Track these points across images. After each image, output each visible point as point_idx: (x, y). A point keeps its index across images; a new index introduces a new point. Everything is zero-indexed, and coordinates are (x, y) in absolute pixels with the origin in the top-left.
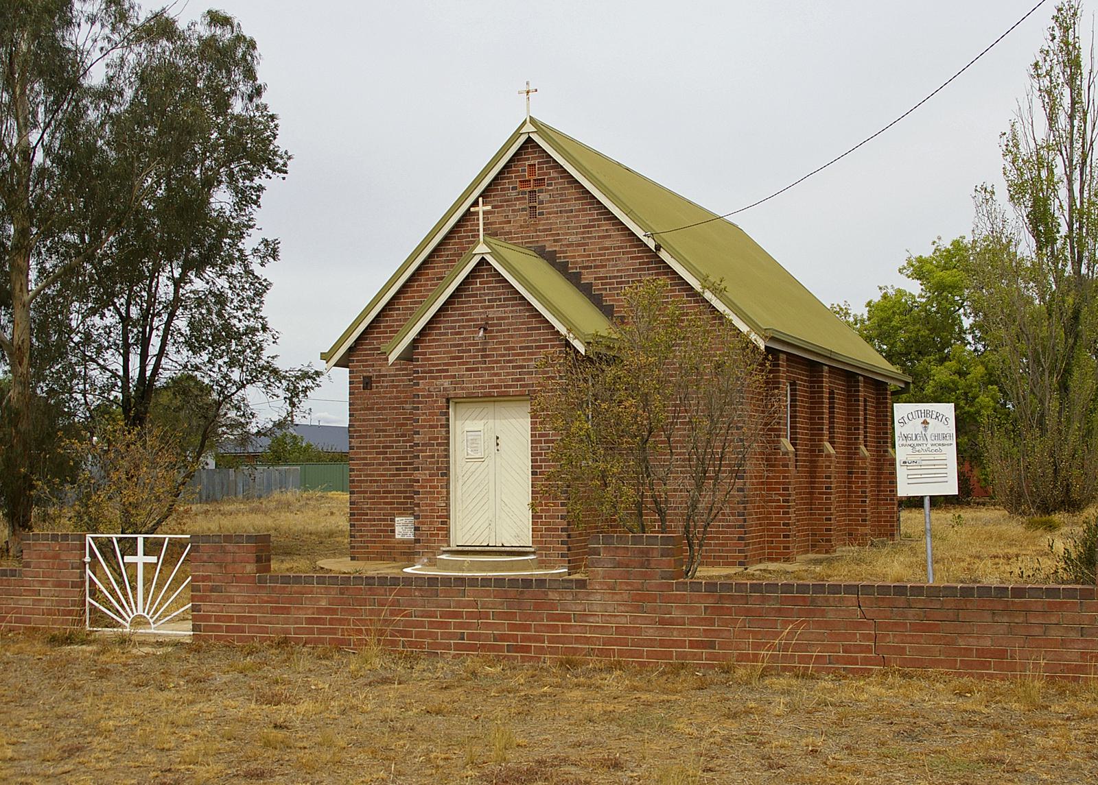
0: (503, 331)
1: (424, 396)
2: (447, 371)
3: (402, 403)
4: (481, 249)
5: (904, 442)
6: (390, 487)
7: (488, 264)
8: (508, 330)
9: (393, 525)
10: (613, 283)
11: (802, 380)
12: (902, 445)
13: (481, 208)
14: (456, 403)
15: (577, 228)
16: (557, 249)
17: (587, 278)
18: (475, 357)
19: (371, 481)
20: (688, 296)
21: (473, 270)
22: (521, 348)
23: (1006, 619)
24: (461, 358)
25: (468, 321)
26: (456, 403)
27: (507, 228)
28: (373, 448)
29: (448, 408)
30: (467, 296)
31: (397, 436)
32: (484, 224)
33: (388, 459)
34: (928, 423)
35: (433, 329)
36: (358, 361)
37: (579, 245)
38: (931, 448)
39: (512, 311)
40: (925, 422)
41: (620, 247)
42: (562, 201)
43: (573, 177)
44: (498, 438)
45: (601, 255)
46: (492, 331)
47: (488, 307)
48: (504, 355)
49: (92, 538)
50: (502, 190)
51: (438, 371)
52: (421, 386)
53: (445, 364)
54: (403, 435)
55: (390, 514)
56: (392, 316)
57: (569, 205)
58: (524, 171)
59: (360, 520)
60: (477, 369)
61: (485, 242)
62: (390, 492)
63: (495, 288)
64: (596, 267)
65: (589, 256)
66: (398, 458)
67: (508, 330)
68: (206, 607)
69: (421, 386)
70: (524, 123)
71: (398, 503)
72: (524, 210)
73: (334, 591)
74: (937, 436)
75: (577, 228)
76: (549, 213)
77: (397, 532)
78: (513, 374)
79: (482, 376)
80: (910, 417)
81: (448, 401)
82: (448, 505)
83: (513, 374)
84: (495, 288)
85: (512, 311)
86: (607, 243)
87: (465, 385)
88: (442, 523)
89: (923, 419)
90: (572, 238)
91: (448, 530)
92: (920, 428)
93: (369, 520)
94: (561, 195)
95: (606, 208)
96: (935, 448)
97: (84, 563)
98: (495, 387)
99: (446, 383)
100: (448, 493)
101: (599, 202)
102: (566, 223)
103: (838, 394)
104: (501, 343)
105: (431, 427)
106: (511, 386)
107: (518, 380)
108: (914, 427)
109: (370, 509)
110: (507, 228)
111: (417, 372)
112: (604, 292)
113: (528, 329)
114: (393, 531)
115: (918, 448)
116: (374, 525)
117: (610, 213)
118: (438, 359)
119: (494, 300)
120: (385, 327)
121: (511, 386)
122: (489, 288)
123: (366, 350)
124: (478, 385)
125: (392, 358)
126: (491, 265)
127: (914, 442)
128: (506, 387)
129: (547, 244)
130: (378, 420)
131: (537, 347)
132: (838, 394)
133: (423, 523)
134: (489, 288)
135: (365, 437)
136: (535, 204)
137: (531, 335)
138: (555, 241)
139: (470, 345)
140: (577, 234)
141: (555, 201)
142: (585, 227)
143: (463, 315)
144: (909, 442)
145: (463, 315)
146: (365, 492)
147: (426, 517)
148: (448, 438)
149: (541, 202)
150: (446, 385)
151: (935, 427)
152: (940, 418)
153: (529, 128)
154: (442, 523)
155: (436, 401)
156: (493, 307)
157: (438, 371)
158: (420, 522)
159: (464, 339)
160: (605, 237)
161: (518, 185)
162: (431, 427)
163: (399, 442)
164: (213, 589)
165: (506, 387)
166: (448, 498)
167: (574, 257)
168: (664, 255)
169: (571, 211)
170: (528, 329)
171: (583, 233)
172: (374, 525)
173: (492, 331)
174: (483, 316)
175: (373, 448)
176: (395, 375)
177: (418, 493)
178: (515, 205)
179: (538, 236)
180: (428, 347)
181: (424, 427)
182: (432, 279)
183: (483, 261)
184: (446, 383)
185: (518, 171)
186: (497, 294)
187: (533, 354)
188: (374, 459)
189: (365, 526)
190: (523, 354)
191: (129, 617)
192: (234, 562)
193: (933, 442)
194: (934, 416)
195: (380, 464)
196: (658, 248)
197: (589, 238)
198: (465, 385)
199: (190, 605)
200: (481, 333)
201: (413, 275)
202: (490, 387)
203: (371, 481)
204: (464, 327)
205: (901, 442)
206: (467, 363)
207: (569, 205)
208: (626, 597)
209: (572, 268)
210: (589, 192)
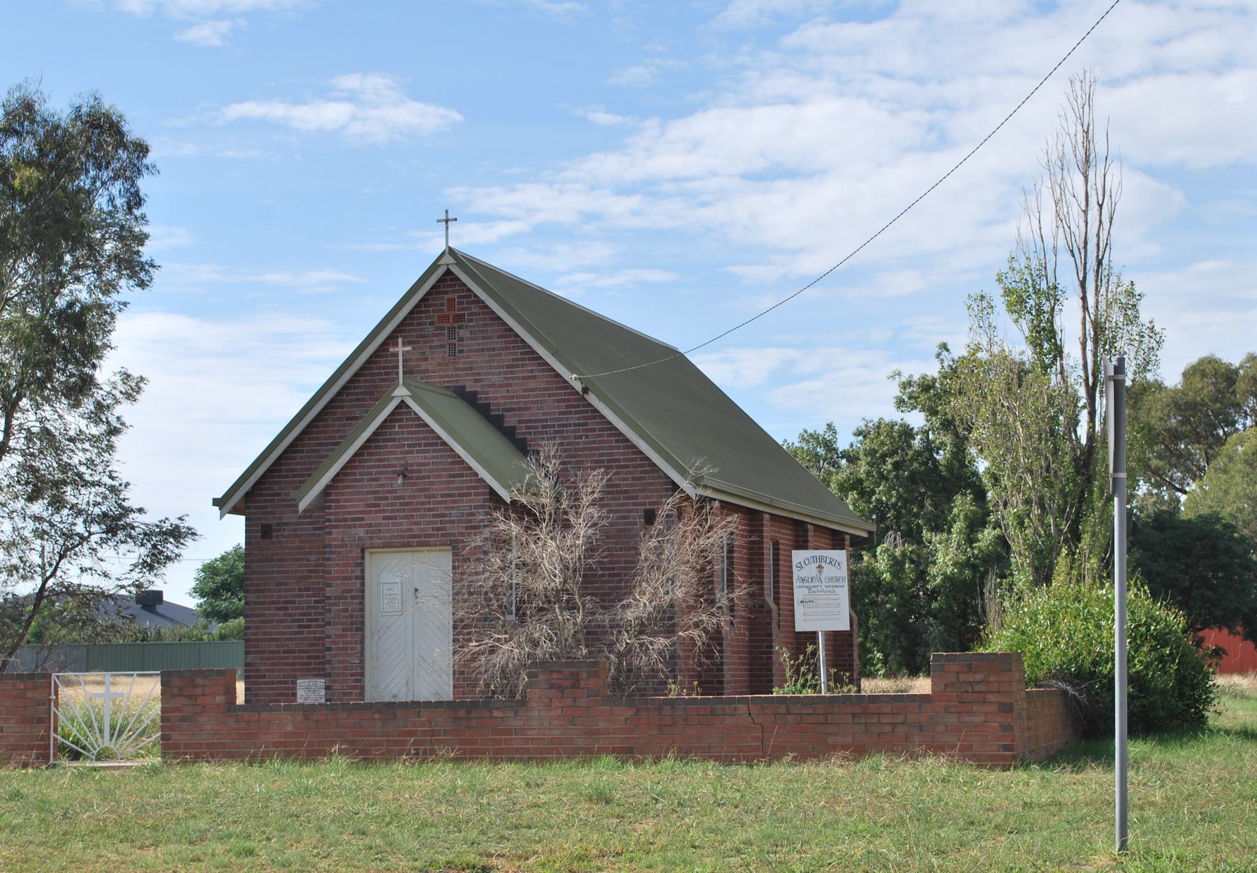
0: (424, 478)
1: (336, 546)
2: (362, 519)
3: (306, 553)
4: (401, 392)
5: (801, 584)
6: (292, 646)
7: (408, 407)
8: (429, 477)
9: (295, 689)
10: (537, 427)
11: (784, 539)
12: (800, 587)
13: (401, 349)
14: (371, 553)
15: (499, 367)
16: (478, 389)
17: (510, 420)
18: (392, 504)
19: (269, 640)
20: (616, 441)
21: (392, 414)
22: (443, 496)
23: (863, 721)
24: (379, 505)
25: (385, 466)
26: (371, 553)
27: (424, 366)
28: (273, 603)
29: (363, 558)
30: (384, 441)
31: (300, 590)
32: (404, 361)
33: (290, 615)
34: (823, 568)
35: (349, 474)
36: (255, 508)
37: (501, 386)
38: (825, 589)
39: (433, 457)
40: (820, 567)
41: (544, 389)
42: (483, 338)
43: (495, 314)
44: (416, 590)
45: (525, 397)
46: (411, 478)
47: (408, 452)
48: (424, 503)
49: (58, 677)
50: (419, 324)
51: (353, 520)
52: (334, 536)
53: (360, 512)
54: (308, 590)
55: (291, 676)
56: (294, 458)
57: (491, 343)
58: (442, 305)
59: (257, 683)
60: (395, 518)
61: (404, 384)
62: (291, 652)
63: (415, 432)
64: (520, 409)
65: (512, 397)
66: (301, 614)
67: (429, 477)
68: (176, 736)
69: (334, 536)
70: (443, 254)
71: (300, 664)
72: (442, 346)
73: (299, 717)
74: (831, 579)
75: (499, 367)
76: (470, 351)
77: (298, 696)
78: (434, 523)
79: (401, 524)
80: (807, 562)
81: (363, 551)
82: (362, 662)
83: (434, 523)
84: (415, 432)
85: (433, 457)
86: (532, 384)
87: (381, 535)
88: (356, 681)
89: (818, 564)
90: (494, 378)
91: (362, 688)
92: (815, 572)
93: (267, 683)
94: (483, 331)
95: (530, 347)
96: (829, 589)
97: (50, 700)
98: (415, 536)
99: (361, 532)
100: (363, 649)
101: (523, 341)
102: (488, 362)
103: (783, 544)
104: (421, 490)
105: (345, 578)
106: (431, 536)
107: (439, 529)
108: (811, 571)
109: (267, 670)
110: (424, 366)
111: (330, 521)
112: (528, 436)
113: (450, 476)
114: (294, 695)
115: (813, 589)
116: (272, 689)
117: (534, 352)
118: (353, 506)
119: (414, 445)
120: (287, 470)
121: (431, 536)
122: (408, 433)
123: (266, 495)
124: (396, 534)
125: (303, 505)
126: (410, 408)
127: (811, 584)
128: (426, 536)
129: (467, 384)
130: (278, 572)
131: (459, 495)
132: (783, 544)
133: (335, 682)
134: (408, 433)
135: (263, 591)
136: (454, 341)
137: (453, 482)
138: (476, 381)
139: (388, 492)
140: (500, 373)
141: (476, 339)
142: (508, 366)
143: (380, 460)
144: (806, 584)
145: (380, 460)
146: (263, 652)
147: (338, 675)
148: (363, 591)
149: (461, 339)
150: (362, 534)
151: (829, 571)
152: (833, 563)
153: (449, 260)
154: (356, 681)
155: (351, 552)
156: (412, 452)
157: (353, 520)
158: (332, 681)
159: (381, 486)
160: (529, 378)
161: (435, 320)
162: (345, 578)
163: (302, 596)
164: (182, 719)
165: (426, 536)
166: (362, 654)
167: (496, 398)
168: (592, 398)
169: (494, 349)
170: (450, 476)
171: (506, 373)
172: (272, 689)
173: (411, 478)
174: (402, 462)
175: (273, 603)
176: (299, 524)
177: (329, 649)
178: (433, 341)
179: (457, 375)
180: (342, 494)
181: (337, 578)
182: (341, 419)
183: (402, 404)
184: (361, 532)
185: (436, 305)
186: (417, 439)
187: (455, 502)
188: (274, 615)
189: (262, 689)
190: (445, 502)
191: (95, 749)
192: (204, 695)
193: (828, 584)
194: (828, 562)
195: (281, 621)
196: (585, 390)
197: (513, 378)
198: (381, 535)
199: (160, 734)
200: (400, 481)
201: (319, 414)
202: (410, 537)
203: (269, 640)
204: (381, 473)
205: (798, 584)
206: (385, 511)
207: (491, 343)
208: (559, 712)
209: (495, 410)
210: (511, 330)
